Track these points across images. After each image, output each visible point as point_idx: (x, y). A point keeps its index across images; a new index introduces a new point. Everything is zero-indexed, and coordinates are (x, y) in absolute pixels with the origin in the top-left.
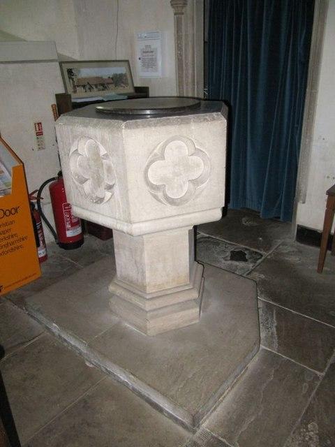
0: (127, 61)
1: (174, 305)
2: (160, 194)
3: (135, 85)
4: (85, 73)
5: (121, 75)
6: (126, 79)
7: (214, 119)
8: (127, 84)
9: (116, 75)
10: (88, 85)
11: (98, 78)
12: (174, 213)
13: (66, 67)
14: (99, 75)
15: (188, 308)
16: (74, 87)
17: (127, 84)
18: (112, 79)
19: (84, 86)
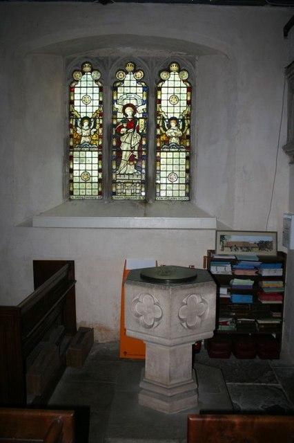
0: (276, 233)
1: (157, 393)
2: (184, 324)
3: (278, 250)
4: (234, 238)
5: (267, 243)
6: (272, 245)
7: (165, 289)
8: (271, 248)
9: (263, 242)
10: (234, 246)
11: (244, 242)
12: (143, 331)
13: (219, 234)
14: (246, 241)
15: (162, 400)
16: (223, 247)
17: (271, 248)
18: (258, 244)
19: (231, 248)
